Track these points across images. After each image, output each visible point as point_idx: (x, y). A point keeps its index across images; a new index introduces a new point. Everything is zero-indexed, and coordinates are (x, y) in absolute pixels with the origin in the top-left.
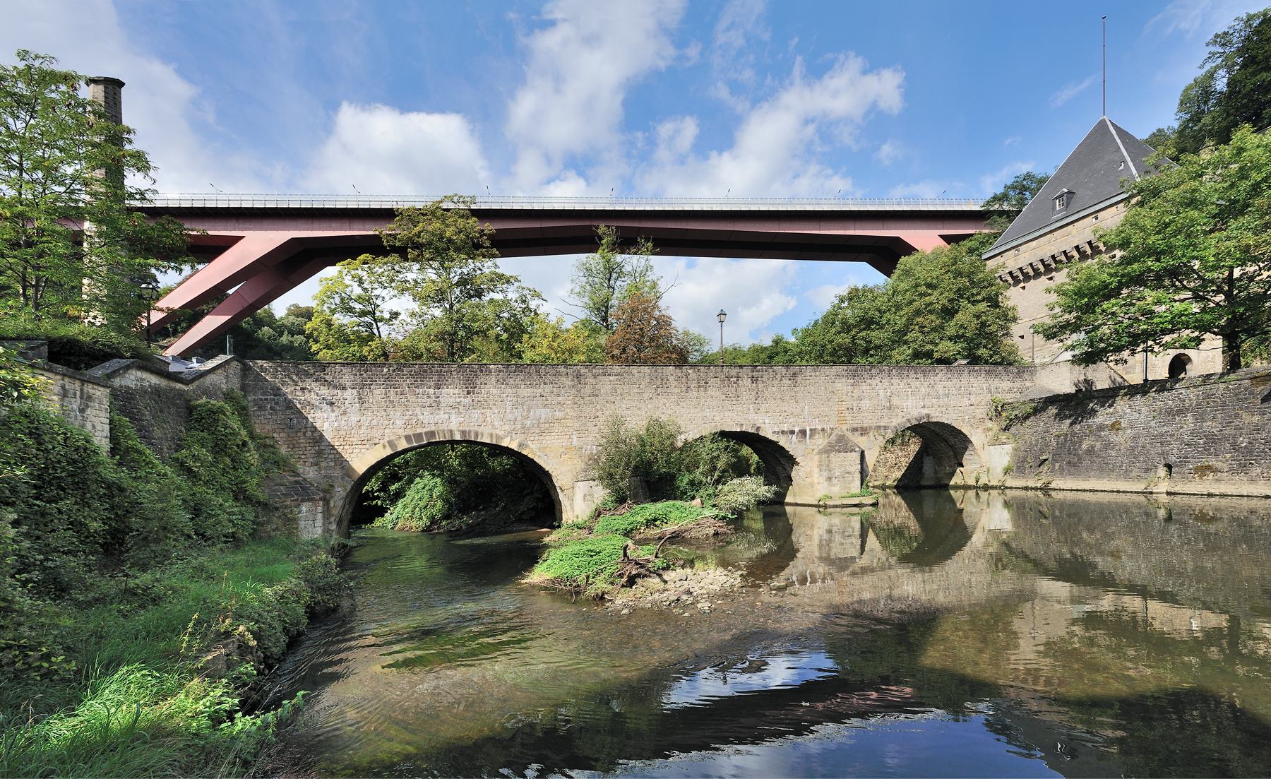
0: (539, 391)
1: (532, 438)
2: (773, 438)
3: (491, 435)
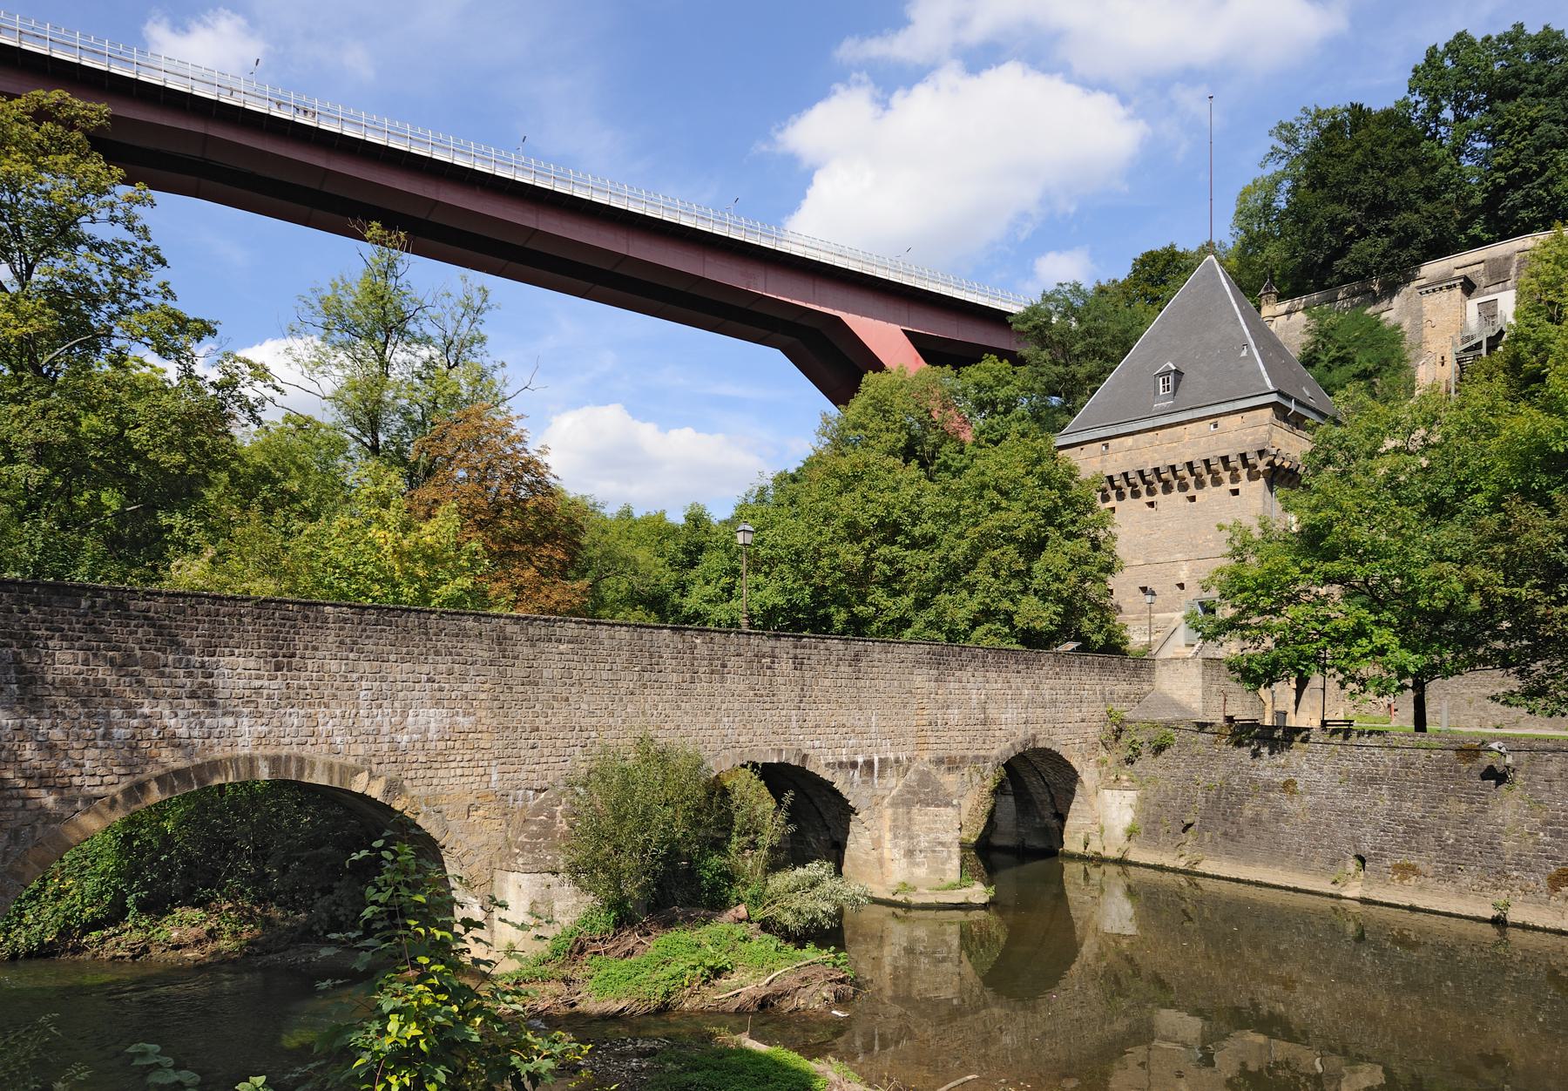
0: (426, 668)
1: (411, 774)
2: (826, 775)
3: (331, 767)
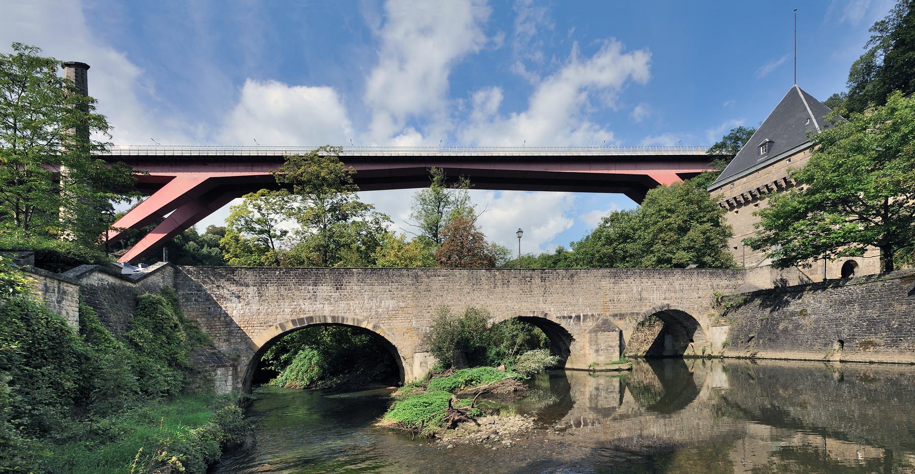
0: (388, 287)
1: (383, 322)
2: (557, 321)
3: (354, 319)
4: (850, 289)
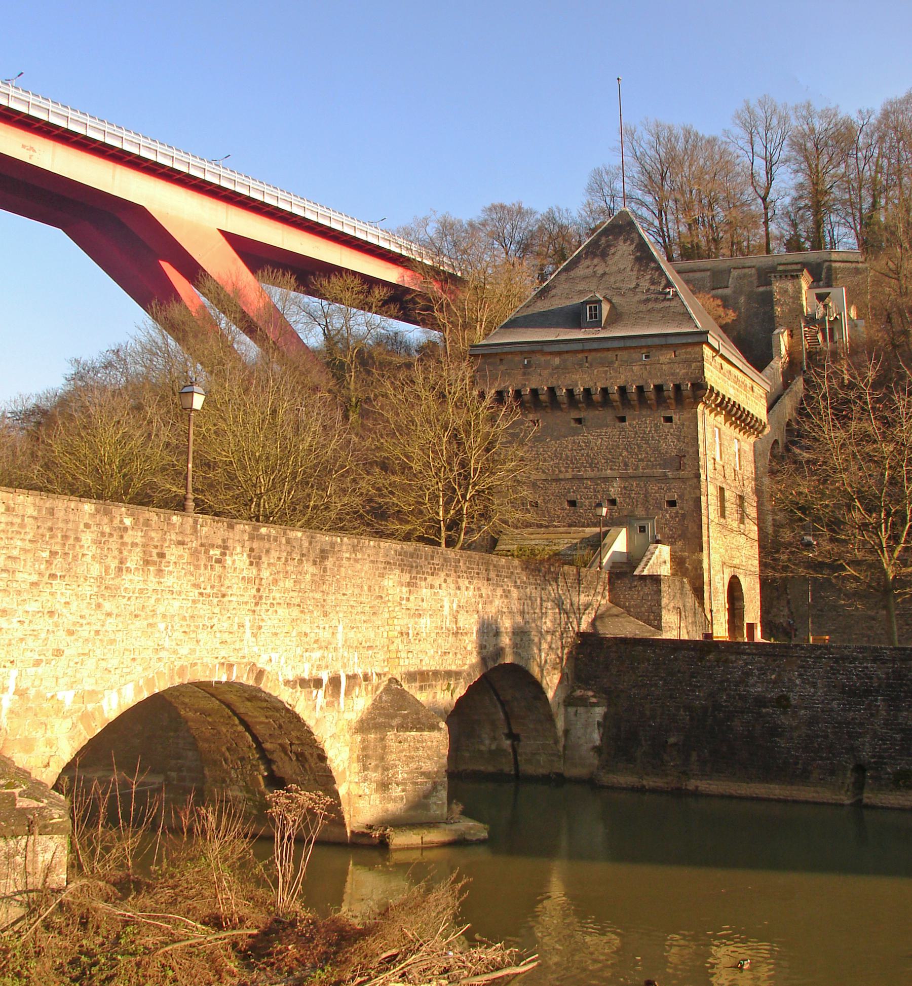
2: (285, 695)
4: (867, 667)
